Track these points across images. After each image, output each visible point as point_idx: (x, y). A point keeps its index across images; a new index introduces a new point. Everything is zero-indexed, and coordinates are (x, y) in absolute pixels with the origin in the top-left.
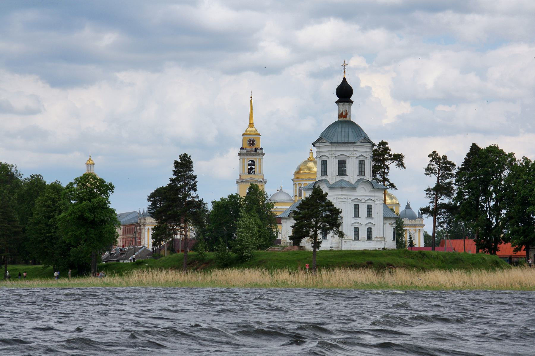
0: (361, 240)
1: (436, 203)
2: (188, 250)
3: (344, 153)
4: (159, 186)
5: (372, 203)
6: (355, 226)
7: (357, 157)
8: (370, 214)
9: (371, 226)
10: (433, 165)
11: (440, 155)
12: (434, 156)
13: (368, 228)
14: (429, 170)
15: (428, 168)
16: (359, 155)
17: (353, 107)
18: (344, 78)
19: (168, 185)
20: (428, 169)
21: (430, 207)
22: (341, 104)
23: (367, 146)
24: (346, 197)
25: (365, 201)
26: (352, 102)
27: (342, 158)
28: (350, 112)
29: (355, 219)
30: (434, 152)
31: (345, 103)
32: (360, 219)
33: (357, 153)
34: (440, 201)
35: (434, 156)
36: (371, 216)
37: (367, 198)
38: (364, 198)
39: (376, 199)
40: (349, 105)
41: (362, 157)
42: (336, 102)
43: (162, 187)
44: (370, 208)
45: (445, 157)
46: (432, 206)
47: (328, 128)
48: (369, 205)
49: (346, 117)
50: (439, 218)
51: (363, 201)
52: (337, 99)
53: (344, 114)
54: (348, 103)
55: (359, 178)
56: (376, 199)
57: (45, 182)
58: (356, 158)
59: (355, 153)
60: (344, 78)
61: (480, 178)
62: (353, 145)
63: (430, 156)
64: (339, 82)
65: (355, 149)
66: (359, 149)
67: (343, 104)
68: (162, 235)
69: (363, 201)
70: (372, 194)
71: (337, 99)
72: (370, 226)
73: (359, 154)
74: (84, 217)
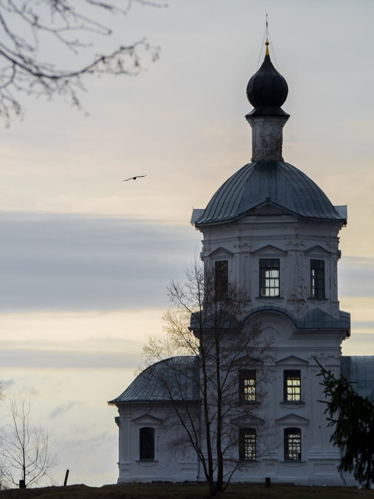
6: (285, 424)
17: (288, 130)
18: (267, 58)
25: (276, 363)
42: (247, 117)
60: (267, 58)
64: (254, 68)
70: (296, 344)
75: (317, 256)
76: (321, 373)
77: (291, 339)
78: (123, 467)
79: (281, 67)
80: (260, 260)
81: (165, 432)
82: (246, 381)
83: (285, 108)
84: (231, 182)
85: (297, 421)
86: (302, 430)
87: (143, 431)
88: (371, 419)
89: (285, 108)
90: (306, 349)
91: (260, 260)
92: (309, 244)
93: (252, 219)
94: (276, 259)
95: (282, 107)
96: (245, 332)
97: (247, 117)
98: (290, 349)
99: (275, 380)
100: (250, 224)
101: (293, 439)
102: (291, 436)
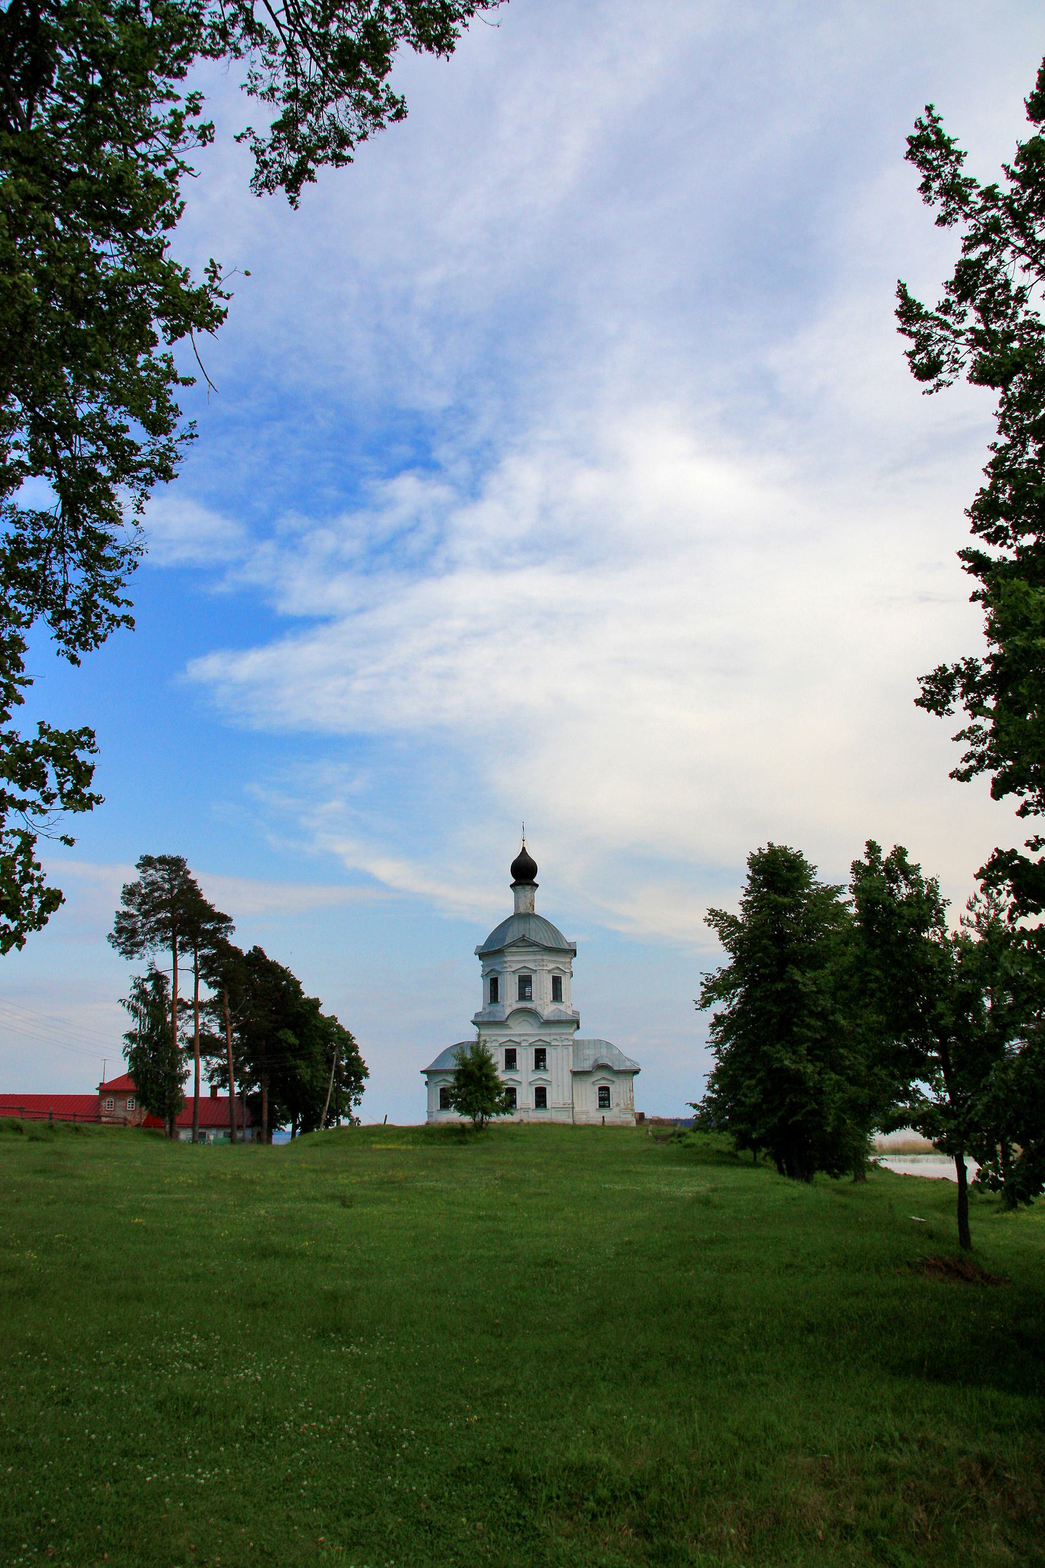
0: (521, 1109)
2: (206, 951)
4: (297, 974)
13: (601, 1089)
18: (524, 849)
22: (519, 888)
24: (557, 1037)
26: (537, 886)
27: (525, 972)
32: (519, 1073)
33: (513, 965)
40: (532, 889)
41: (525, 970)
42: (511, 886)
43: (978, 551)
52: (513, 880)
57: (315, 1004)
60: (524, 849)
64: (515, 854)
70: (542, 1031)
71: (513, 880)
75: (557, 973)
77: (539, 1028)
78: (430, 1113)
79: (533, 854)
82: (188, 1089)
85: (542, 1082)
87: (537, 1051)
88: (913, 1217)
89: (535, 880)
90: (550, 1034)
92: (551, 966)
93: (514, 949)
96: (851, 1548)
97: (511, 886)
98: (538, 1035)
99: (216, 276)
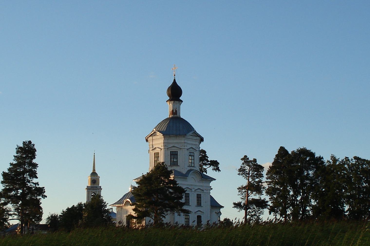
1: (248, 199)
3: (176, 145)
5: (190, 191)
6: (198, 214)
7: (187, 149)
8: (199, 204)
9: (200, 214)
10: (244, 167)
11: (251, 159)
12: (245, 159)
13: (198, 216)
14: (242, 171)
15: (241, 169)
16: (189, 148)
17: (182, 106)
18: (175, 80)
19: (34, 145)
20: (240, 170)
21: (241, 203)
23: (196, 139)
25: (195, 190)
26: (182, 101)
27: (174, 149)
28: (179, 110)
29: (199, 207)
30: (246, 156)
31: (176, 102)
34: (250, 198)
35: (245, 159)
36: (188, 203)
37: (196, 188)
38: (194, 187)
39: (205, 189)
40: (179, 103)
44: (199, 197)
45: (255, 160)
46: (243, 202)
47: (165, 120)
48: (198, 194)
49: (176, 114)
50: (249, 212)
51: (193, 190)
53: (174, 111)
54: (178, 102)
55: (189, 169)
56: (205, 189)
58: (186, 149)
59: (185, 145)
60: (175, 80)
61: (357, 186)
62: (184, 138)
63: (242, 159)
64: (170, 83)
65: (186, 141)
66: (189, 142)
67: (174, 103)
68: (118, 227)
69: (193, 190)
70: (201, 184)
72: (199, 214)
73: (189, 146)
74: (100, 198)
76: (194, 191)
80: (170, 152)
81: (170, 223)
83: (181, 98)
84: (161, 124)
86: (202, 216)
89: (181, 98)
91: (170, 152)
94: (176, 151)
95: (180, 98)
100: (187, 138)
101: (267, 244)
102: (266, 244)
